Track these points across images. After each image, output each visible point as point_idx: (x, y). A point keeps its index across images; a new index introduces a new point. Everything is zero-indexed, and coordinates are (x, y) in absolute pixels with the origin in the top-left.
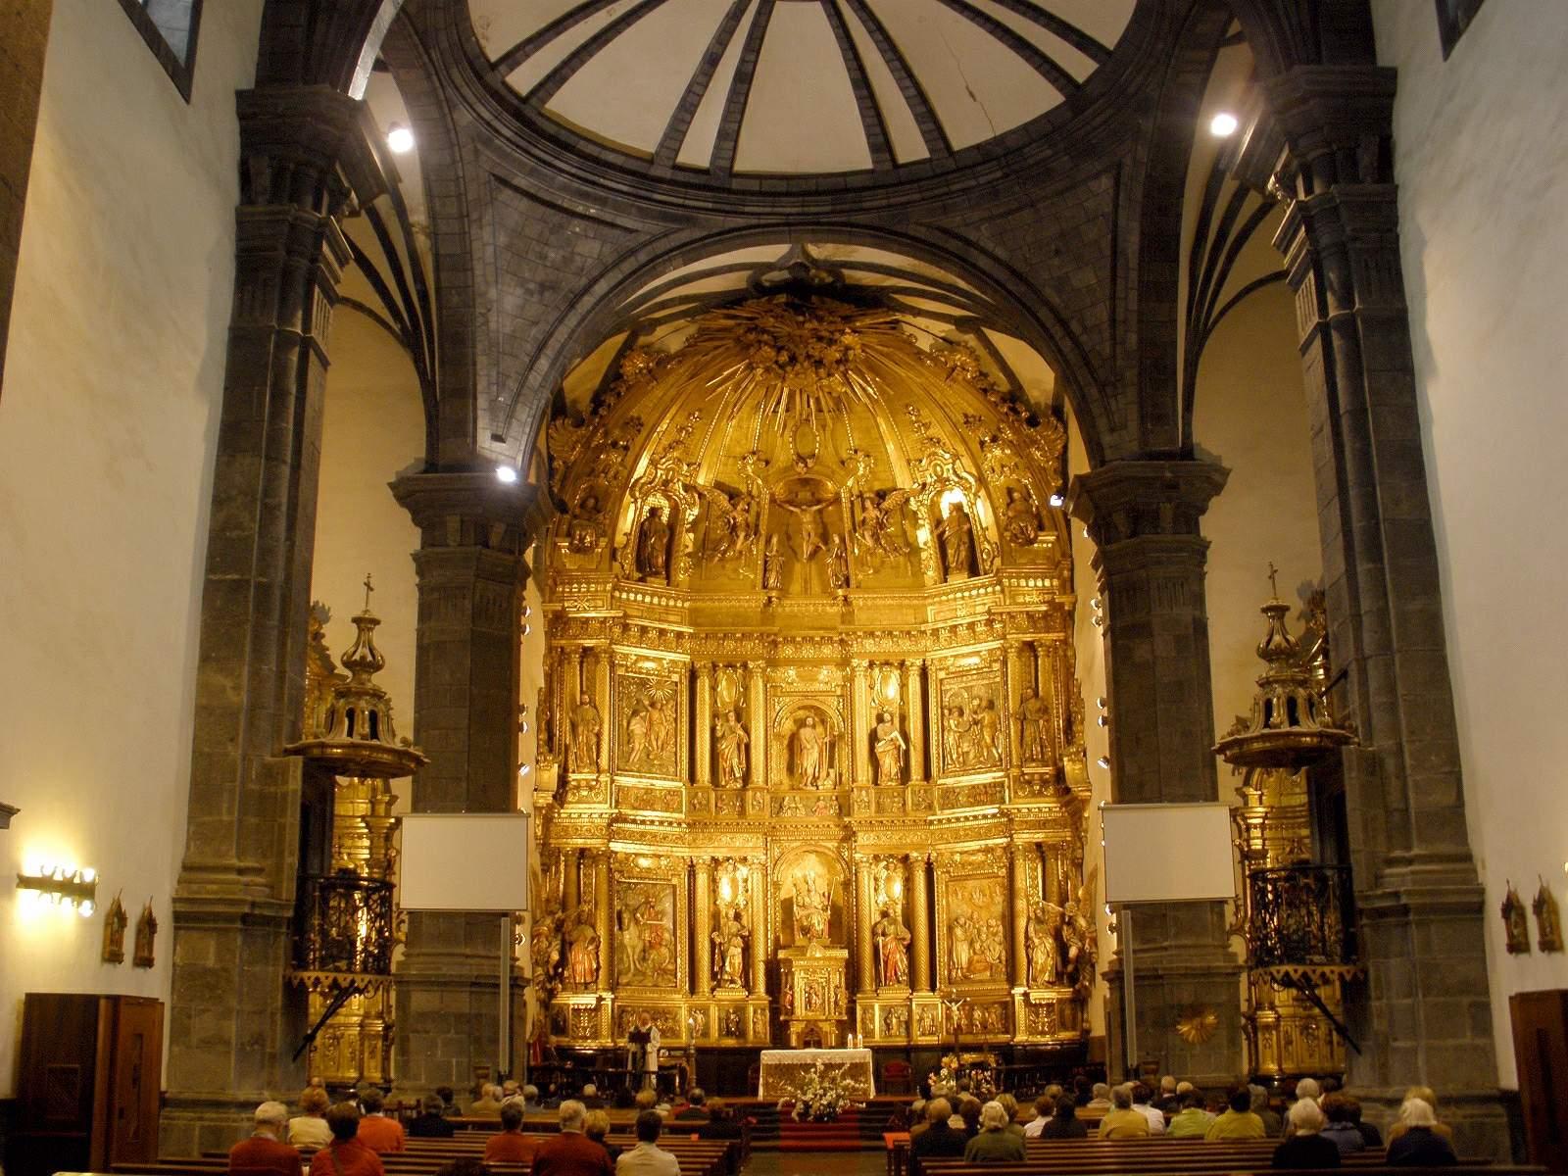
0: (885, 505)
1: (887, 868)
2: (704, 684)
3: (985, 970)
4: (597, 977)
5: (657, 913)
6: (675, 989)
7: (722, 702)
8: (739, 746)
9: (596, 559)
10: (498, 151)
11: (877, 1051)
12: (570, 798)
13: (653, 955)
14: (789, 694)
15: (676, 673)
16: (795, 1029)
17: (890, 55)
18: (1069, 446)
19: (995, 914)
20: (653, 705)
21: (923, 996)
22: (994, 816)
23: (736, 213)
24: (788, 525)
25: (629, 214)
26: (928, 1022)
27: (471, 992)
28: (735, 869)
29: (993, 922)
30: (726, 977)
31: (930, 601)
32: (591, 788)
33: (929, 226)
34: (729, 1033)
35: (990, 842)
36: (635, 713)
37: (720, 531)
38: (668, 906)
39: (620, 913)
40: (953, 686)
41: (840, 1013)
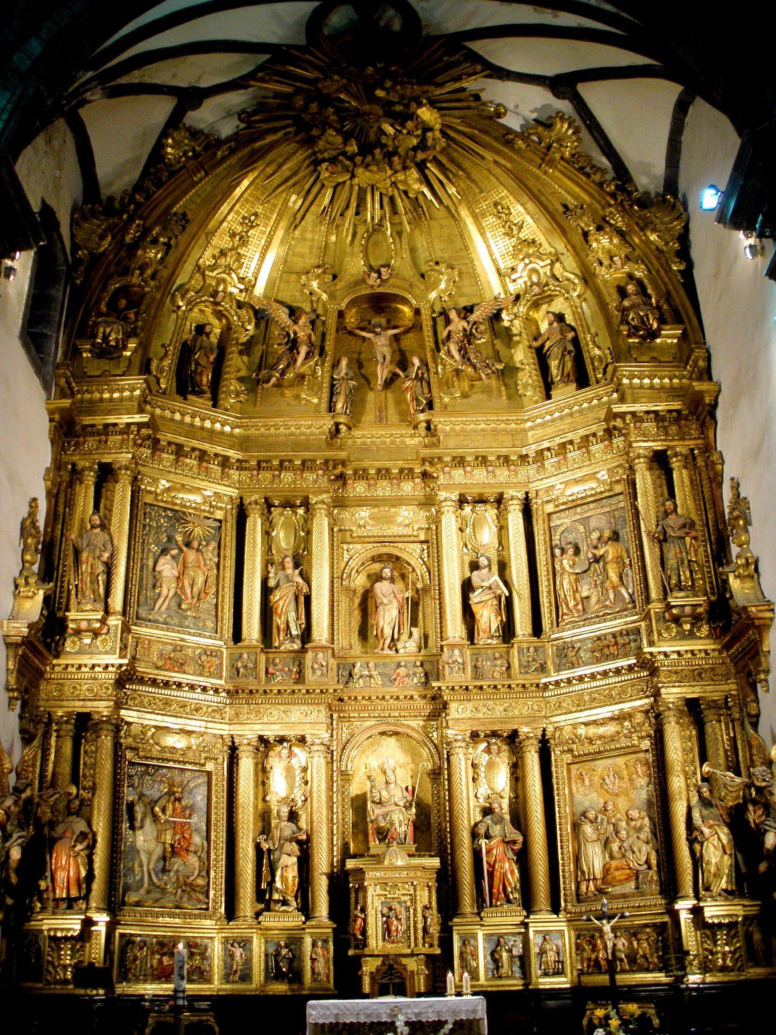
0: (473, 318)
1: (488, 751)
2: (255, 525)
3: (627, 879)
4: (89, 890)
5: (184, 809)
6: (206, 911)
7: (279, 551)
8: (297, 598)
11: (495, 1000)
12: (69, 646)
13: (177, 864)
14: (362, 540)
15: (220, 508)
16: (369, 966)
18: (691, 226)
19: (637, 803)
20: (188, 545)
21: (544, 922)
22: (630, 668)
24: (360, 353)
26: (551, 956)
28: (291, 754)
29: (635, 814)
30: (276, 896)
31: (529, 424)
32: (96, 634)
34: (279, 976)
35: (626, 706)
36: (164, 551)
37: (279, 348)
38: (200, 798)
39: (131, 806)
40: (563, 521)
41: (431, 945)
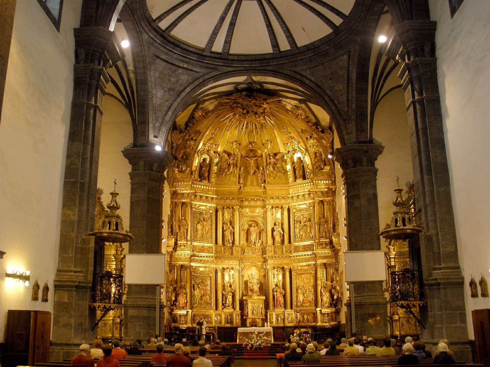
0: (277, 158)
1: (277, 271)
2: (220, 213)
3: (308, 303)
4: (187, 305)
5: (205, 285)
6: (211, 309)
7: (226, 219)
8: (231, 233)
9: (186, 175)
10: (156, 47)
12: (178, 249)
13: (204, 298)
14: (247, 217)
15: (211, 210)
16: (249, 321)
17: (278, 17)
18: (334, 139)
19: (311, 285)
20: (204, 220)
21: (289, 311)
22: (311, 255)
23: (230, 66)
24: (246, 164)
25: (197, 67)
26: (290, 319)
27: (147, 310)
28: (230, 271)
29: (310, 288)
30: (227, 305)
31: (291, 187)
32: (185, 246)
33: (290, 71)
34: (228, 322)
35: (309, 263)
36: (198, 222)
37: (225, 166)
38: (209, 283)
39: (194, 285)
40: (298, 214)
41: (263, 316)
